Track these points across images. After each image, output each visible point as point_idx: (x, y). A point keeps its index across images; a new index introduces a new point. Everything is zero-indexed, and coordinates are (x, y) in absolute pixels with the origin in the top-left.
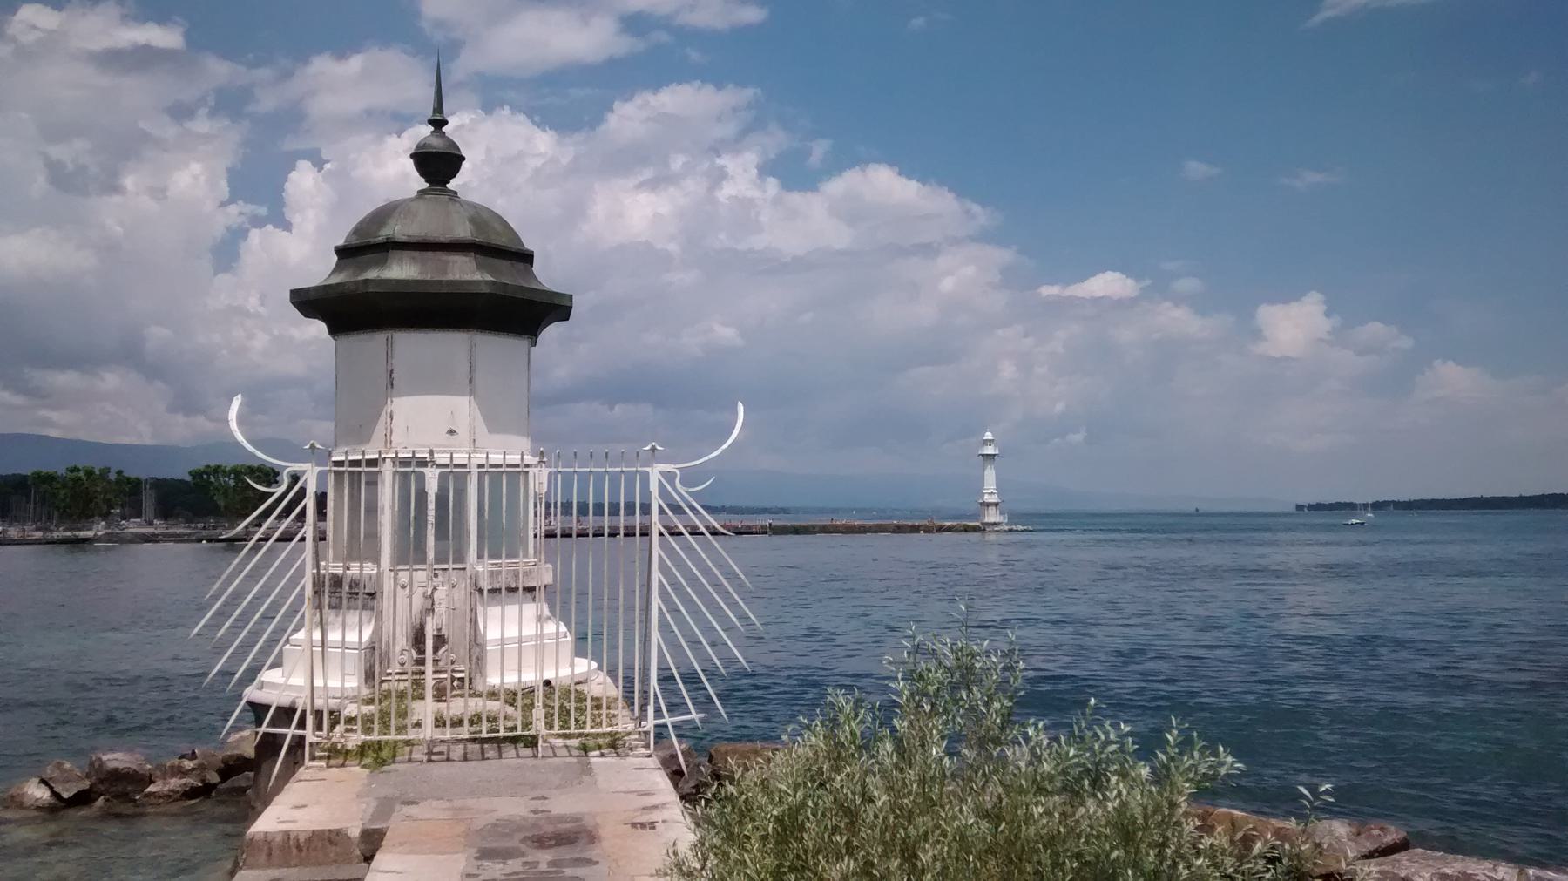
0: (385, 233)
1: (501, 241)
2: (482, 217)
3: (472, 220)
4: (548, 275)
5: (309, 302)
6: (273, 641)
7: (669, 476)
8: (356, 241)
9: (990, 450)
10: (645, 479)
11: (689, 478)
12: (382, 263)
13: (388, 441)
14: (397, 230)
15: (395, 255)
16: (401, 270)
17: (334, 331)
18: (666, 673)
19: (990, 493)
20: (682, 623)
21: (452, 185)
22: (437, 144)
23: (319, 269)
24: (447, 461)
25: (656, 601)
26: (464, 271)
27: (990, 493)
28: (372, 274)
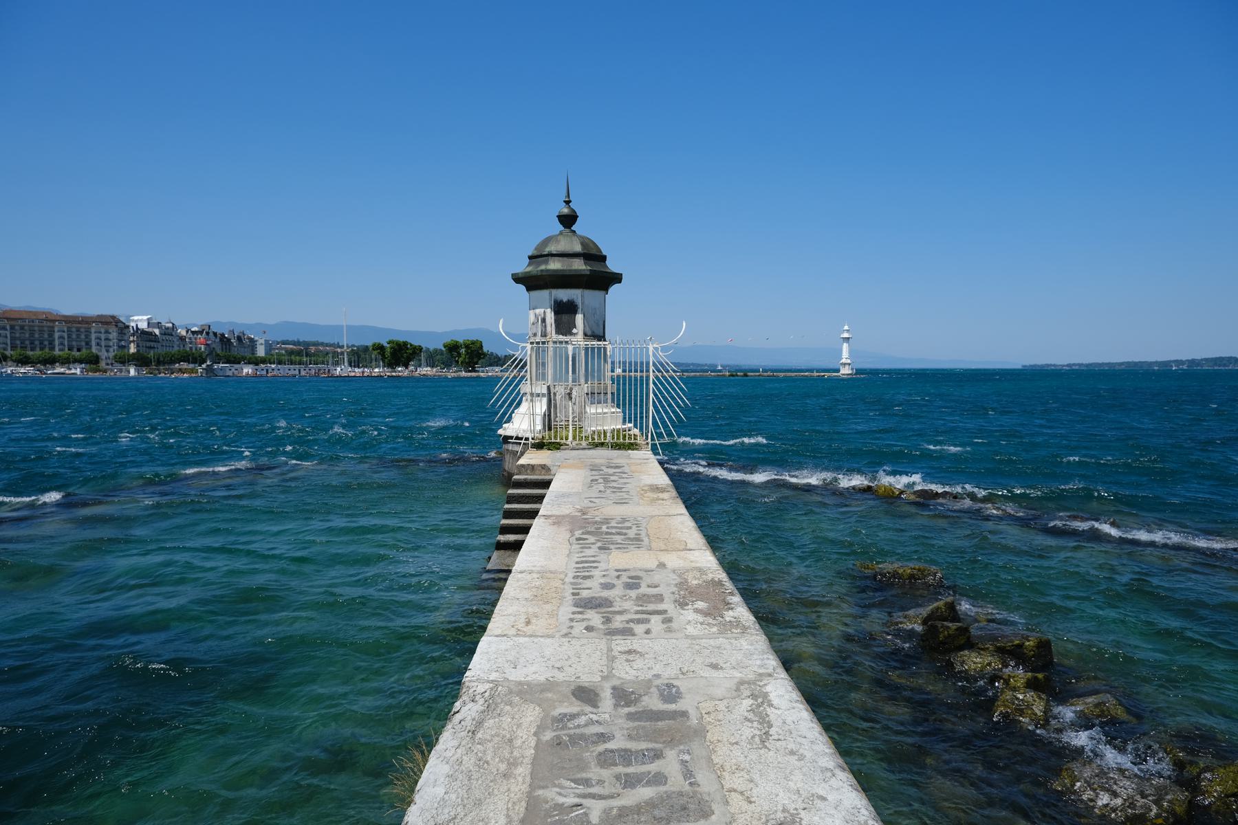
0: (547, 250)
1: (594, 252)
2: (585, 242)
3: (582, 244)
4: (613, 265)
5: (518, 279)
6: (504, 414)
7: (656, 349)
8: (536, 253)
9: (846, 335)
10: (647, 349)
11: (664, 349)
12: (546, 263)
13: (522, 338)
14: (552, 248)
15: (551, 259)
16: (555, 265)
17: (528, 290)
18: (565, 317)
19: (845, 356)
20: (660, 402)
21: (573, 228)
22: (566, 211)
23: (522, 267)
24: (545, 400)
25: (651, 395)
26: (579, 265)
27: (845, 356)
28: (543, 267)
